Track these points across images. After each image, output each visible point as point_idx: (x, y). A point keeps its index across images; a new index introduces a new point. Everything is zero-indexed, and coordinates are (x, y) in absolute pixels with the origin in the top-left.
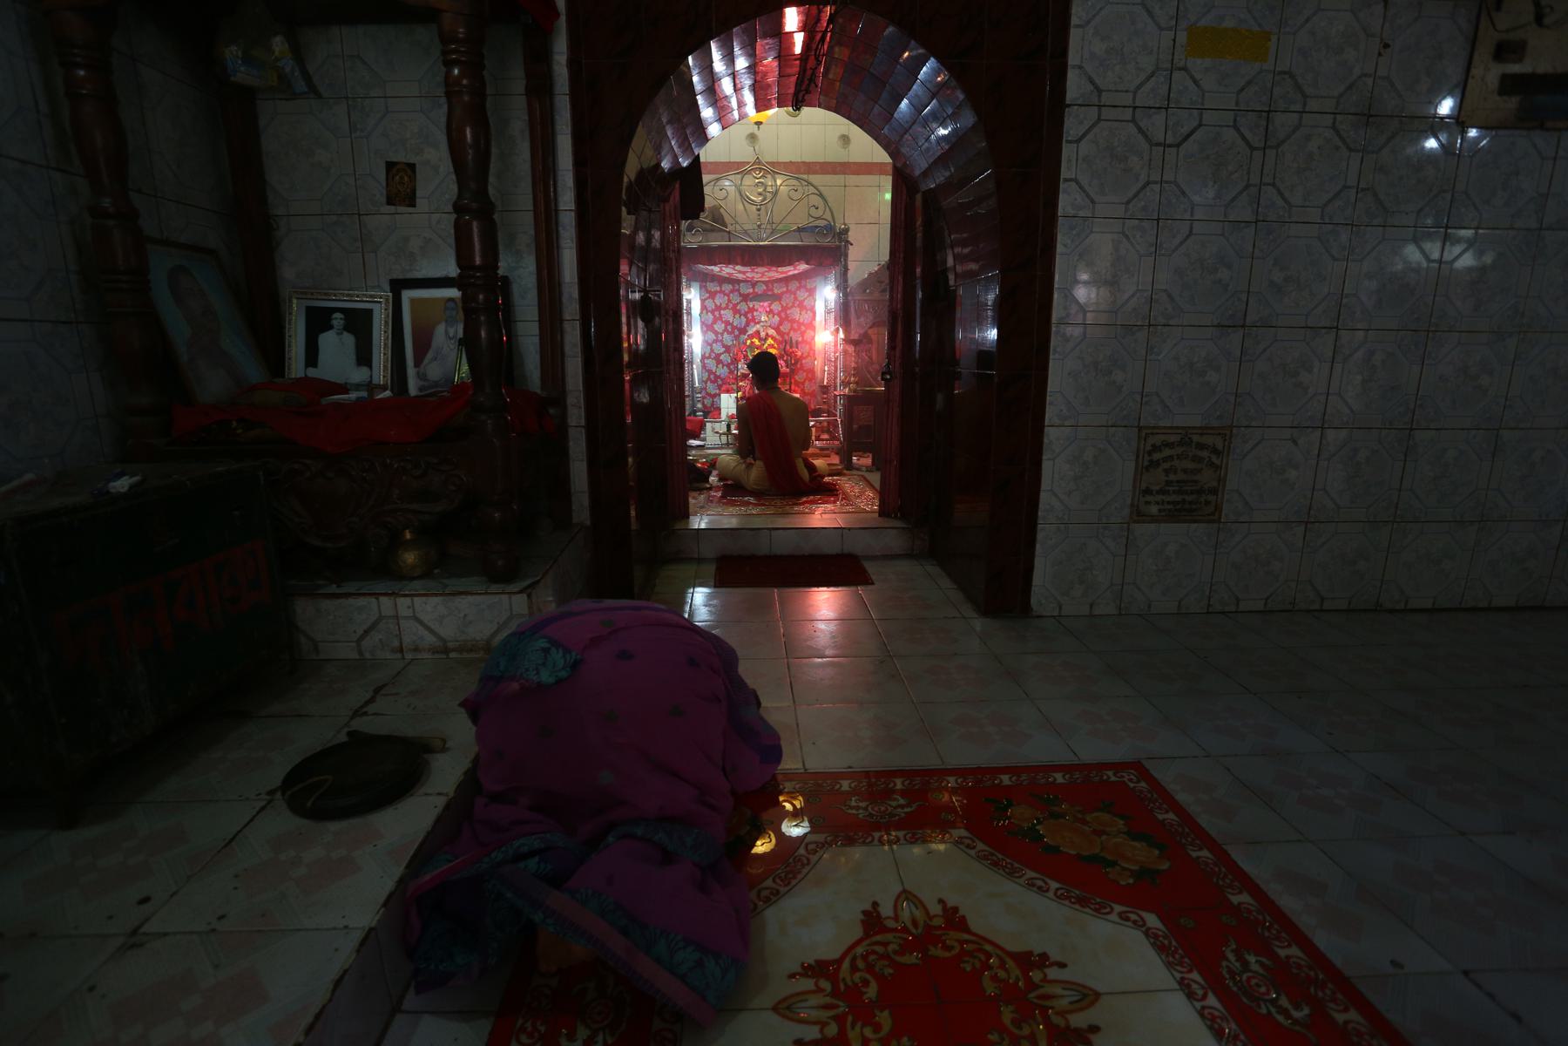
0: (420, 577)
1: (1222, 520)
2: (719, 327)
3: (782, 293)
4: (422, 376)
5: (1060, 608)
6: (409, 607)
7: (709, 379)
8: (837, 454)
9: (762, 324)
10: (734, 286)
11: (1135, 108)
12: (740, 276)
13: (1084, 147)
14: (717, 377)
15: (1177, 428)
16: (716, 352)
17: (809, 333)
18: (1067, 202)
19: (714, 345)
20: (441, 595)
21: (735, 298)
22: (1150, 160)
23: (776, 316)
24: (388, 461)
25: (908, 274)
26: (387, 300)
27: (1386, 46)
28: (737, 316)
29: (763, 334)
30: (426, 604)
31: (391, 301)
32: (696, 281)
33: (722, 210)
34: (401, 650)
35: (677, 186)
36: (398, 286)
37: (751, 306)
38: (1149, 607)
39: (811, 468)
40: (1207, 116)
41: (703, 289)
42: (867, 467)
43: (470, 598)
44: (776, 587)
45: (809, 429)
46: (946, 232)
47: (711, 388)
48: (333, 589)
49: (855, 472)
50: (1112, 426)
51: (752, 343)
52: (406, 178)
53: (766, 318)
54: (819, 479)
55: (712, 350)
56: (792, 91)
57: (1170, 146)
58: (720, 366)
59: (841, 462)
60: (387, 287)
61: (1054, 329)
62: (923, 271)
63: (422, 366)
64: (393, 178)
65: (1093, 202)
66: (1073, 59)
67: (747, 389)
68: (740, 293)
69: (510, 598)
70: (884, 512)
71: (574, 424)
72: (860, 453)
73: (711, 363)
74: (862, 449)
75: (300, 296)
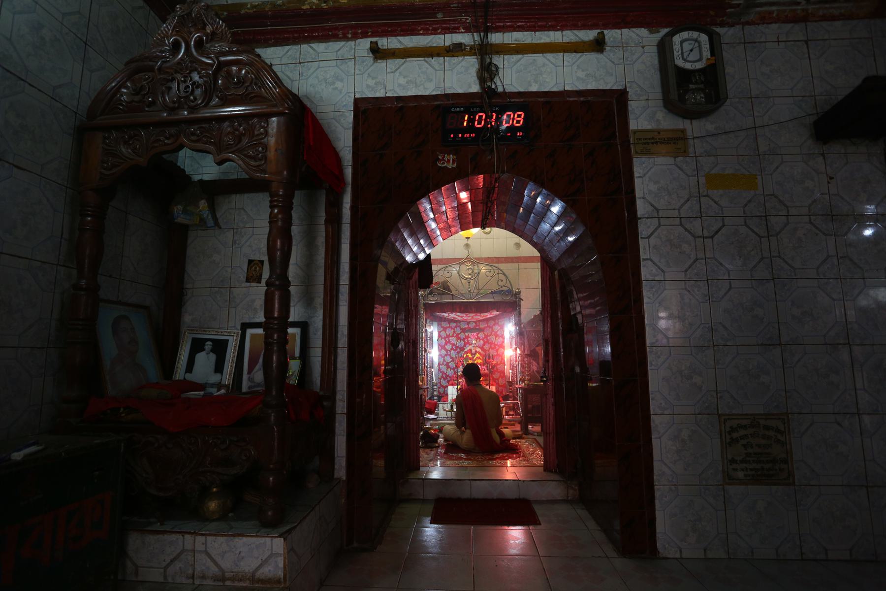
0: (218, 520)
1: (796, 484)
2: (449, 347)
3: (485, 328)
4: (251, 380)
5: (681, 551)
6: (203, 544)
7: (442, 377)
8: (519, 423)
9: (473, 345)
10: (457, 324)
11: (681, 218)
12: (460, 319)
13: (652, 240)
14: (447, 376)
15: (746, 415)
16: (447, 361)
17: (501, 350)
18: (647, 271)
19: (446, 357)
20: (226, 535)
21: (458, 331)
22: (696, 246)
23: (481, 341)
24: (207, 438)
25: (553, 317)
26: (238, 335)
27: (831, 178)
28: (459, 340)
29: (473, 351)
30: (215, 542)
31: (240, 335)
32: (436, 321)
33: (448, 283)
34: (193, 577)
35: (417, 270)
36: (245, 326)
37: (467, 335)
38: (752, 553)
39: (501, 435)
40: (726, 220)
41: (440, 326)
42: (537, 433)
43: (245, 539)
44: (472, 525)
45: (500, 408)
46: (575, 293)
47: (444, 383)
48: (158, 527)
49: (530, 436)
50: (698, 414)
51: (467, 356)
52: (258, 268)
53: (476, 342)
54: (506, 442)
55: (444, 360)
56: (480, 219)
57: (706, 238)
58: (449, 369)
59: (521, 429)
60: (239, 327)
61: (648, 350)
62: (562, 315)
63: (252, 374)
64: (251, 269)
65: (663, 271)
66: (638, 193)
67: (464, 384)
68: (460, 328)
69: (272, 540)
70: (547, 468)
71: (340, 412)
72: (534, 424)
73: (443, 368)
74: (534, 422)
75: (190, 332)
